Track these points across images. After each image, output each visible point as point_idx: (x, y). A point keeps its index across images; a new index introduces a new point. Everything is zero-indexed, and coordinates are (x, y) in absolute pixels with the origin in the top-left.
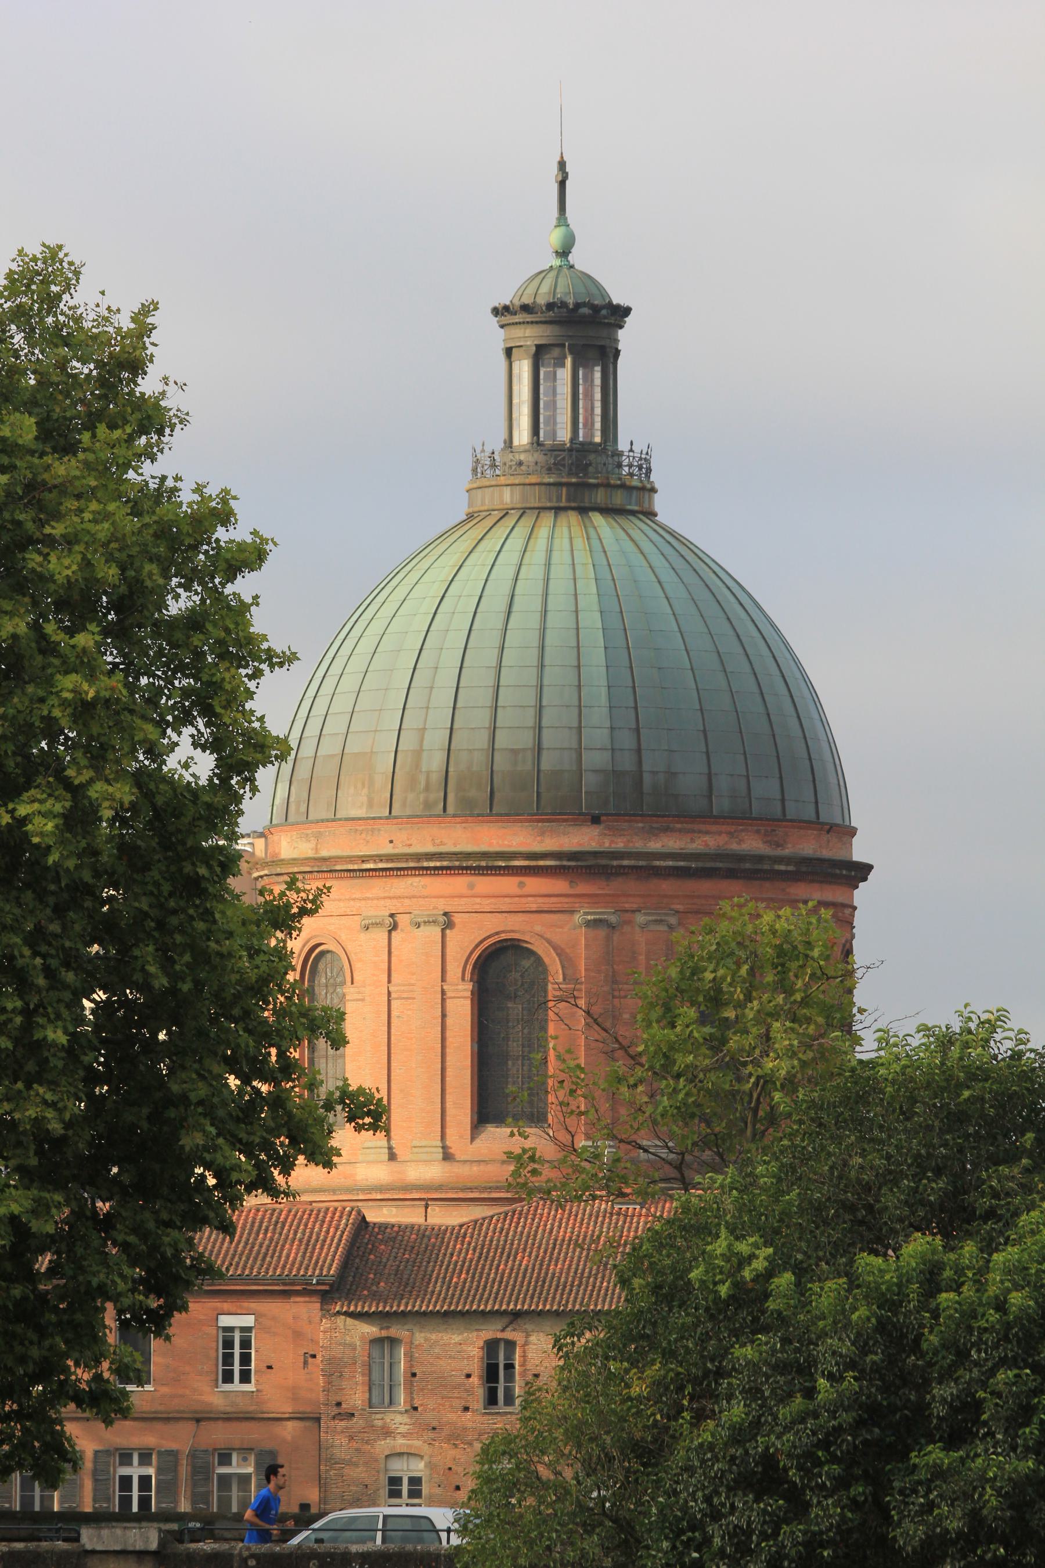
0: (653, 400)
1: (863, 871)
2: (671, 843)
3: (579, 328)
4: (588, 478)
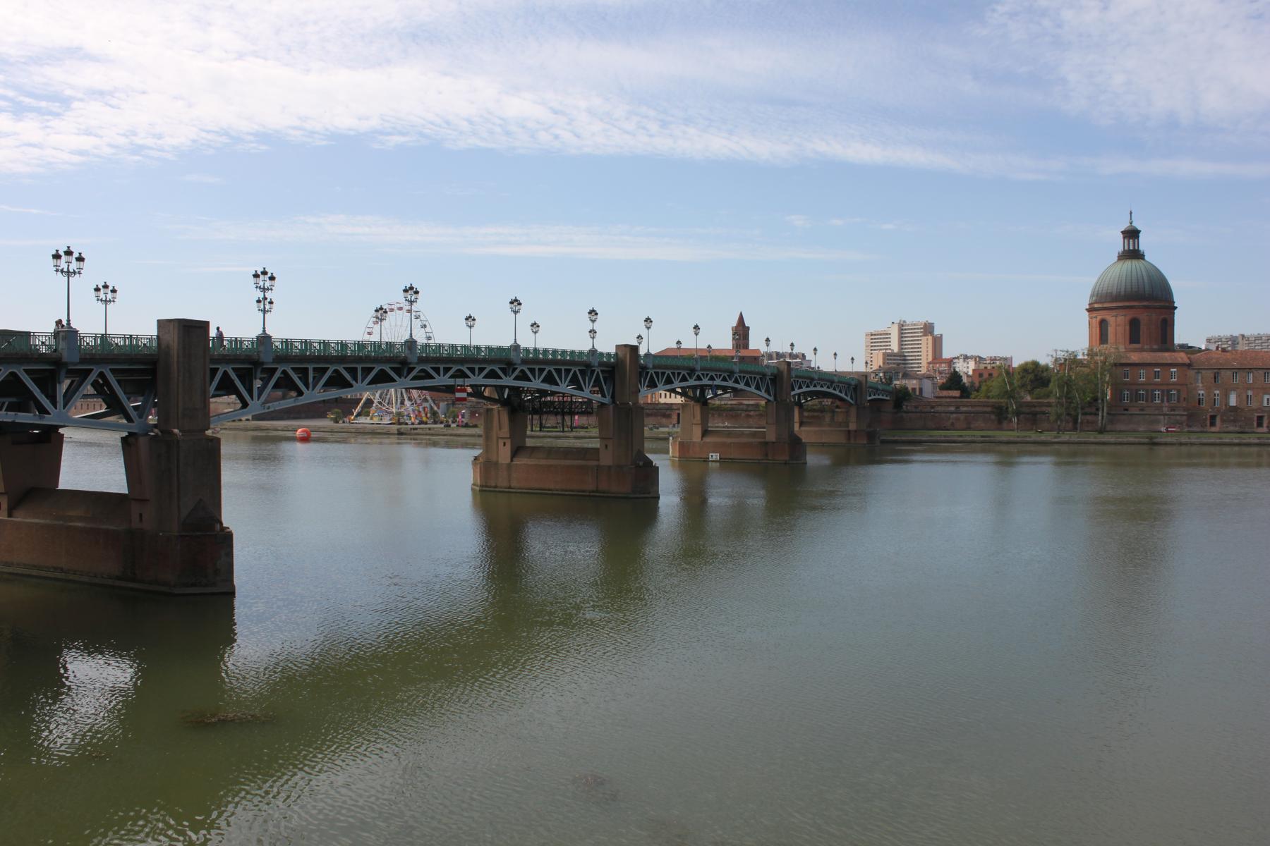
0: (1144, 243)
3: (1132, 234)
4: (1133, 254)
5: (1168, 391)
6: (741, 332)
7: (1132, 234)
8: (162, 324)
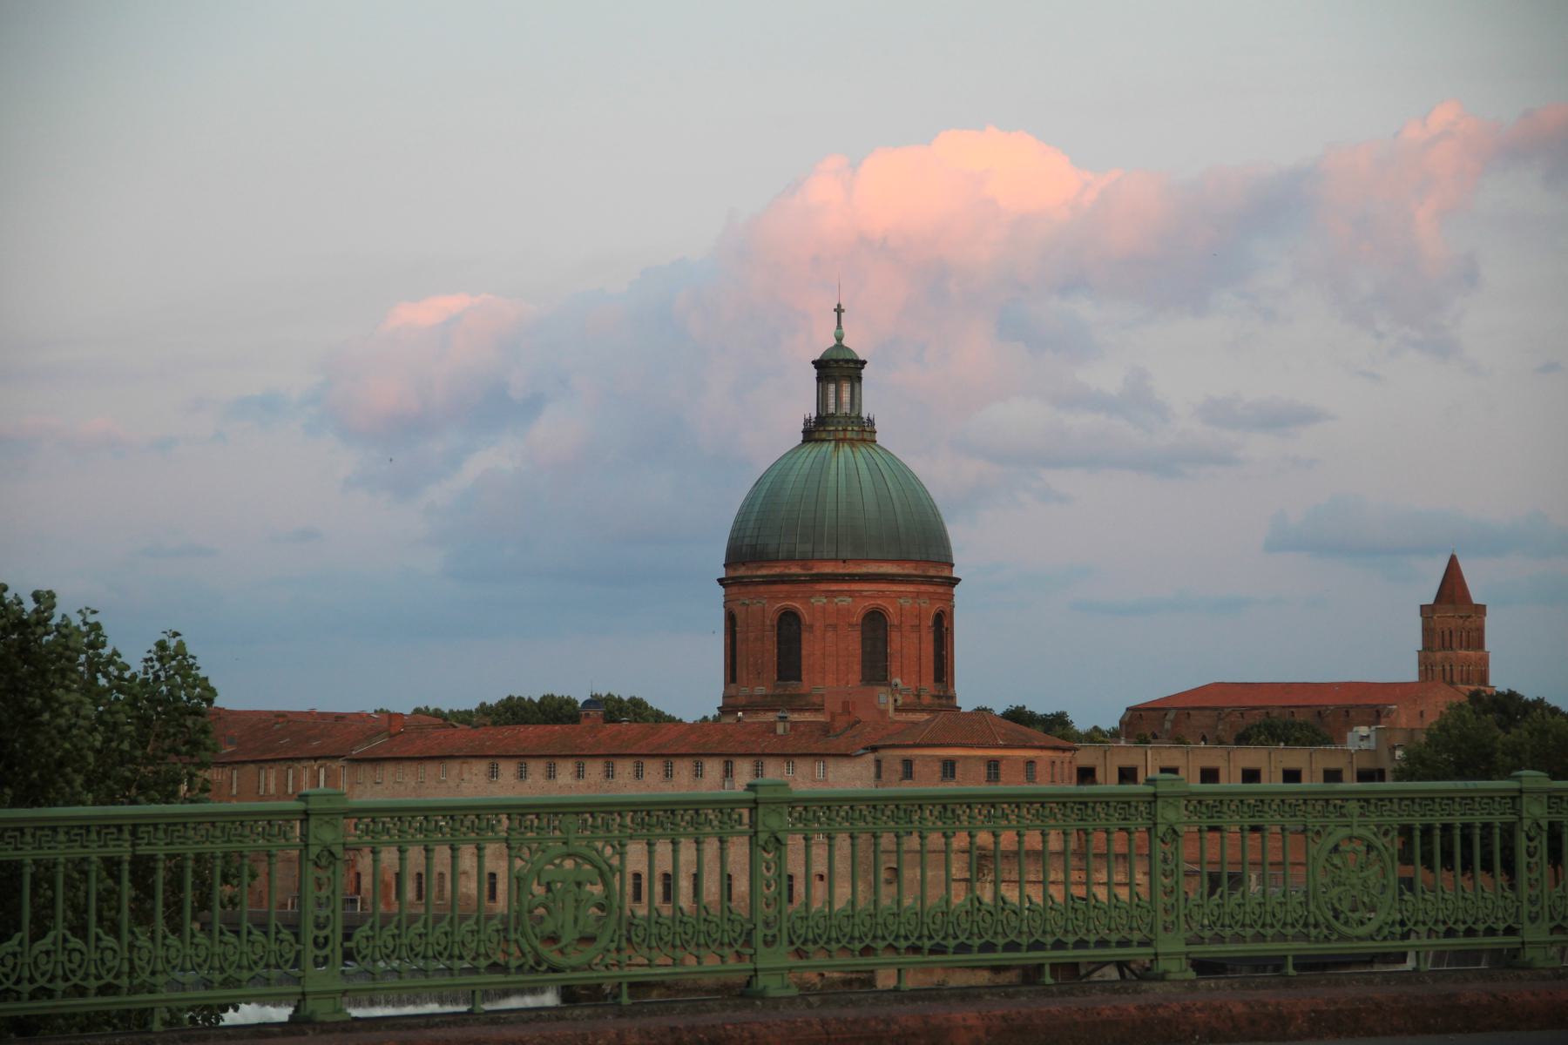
0: (876, 398)
1: (958, 580)
2: (764, 572)
3: (838, 369)
6: (1452, 616)
7: (838, 369)
8: (170, 654)
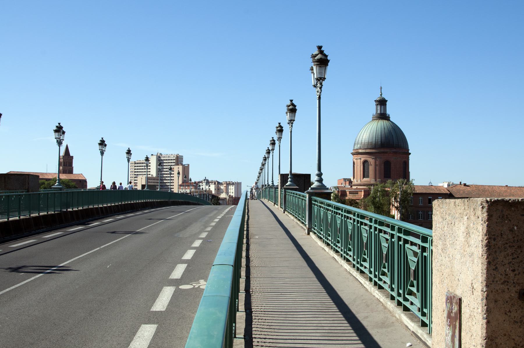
0: (389, 111)
3: (382, 102)
4: (383, 116)
5: (418, 211)
